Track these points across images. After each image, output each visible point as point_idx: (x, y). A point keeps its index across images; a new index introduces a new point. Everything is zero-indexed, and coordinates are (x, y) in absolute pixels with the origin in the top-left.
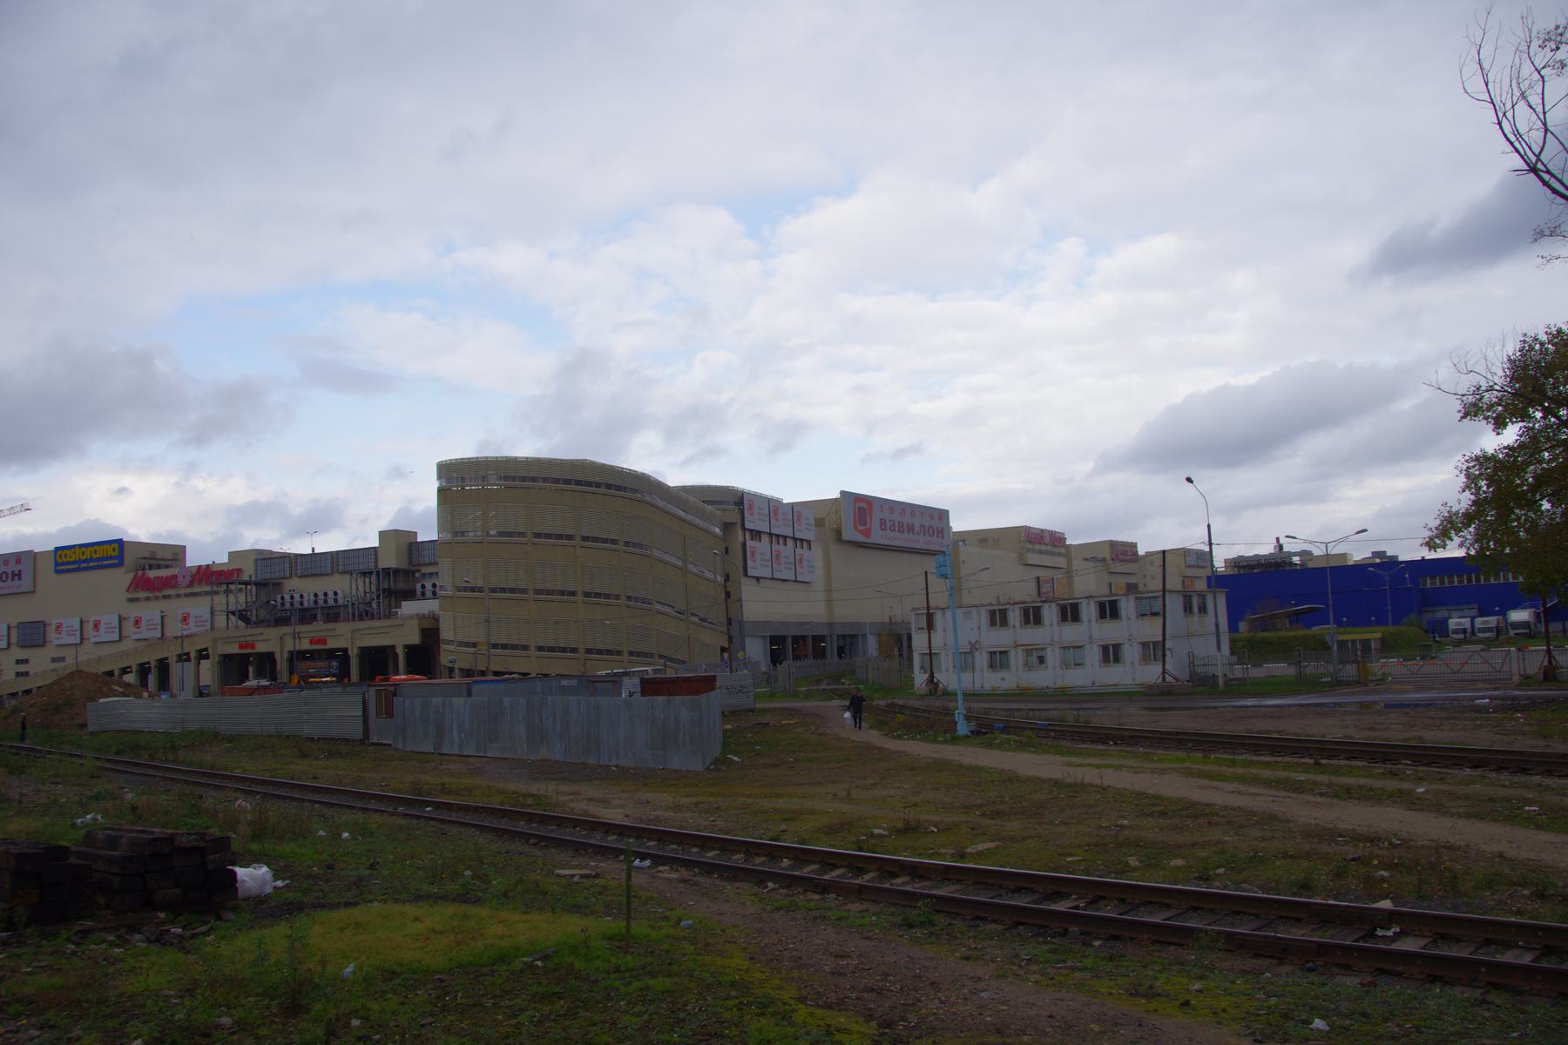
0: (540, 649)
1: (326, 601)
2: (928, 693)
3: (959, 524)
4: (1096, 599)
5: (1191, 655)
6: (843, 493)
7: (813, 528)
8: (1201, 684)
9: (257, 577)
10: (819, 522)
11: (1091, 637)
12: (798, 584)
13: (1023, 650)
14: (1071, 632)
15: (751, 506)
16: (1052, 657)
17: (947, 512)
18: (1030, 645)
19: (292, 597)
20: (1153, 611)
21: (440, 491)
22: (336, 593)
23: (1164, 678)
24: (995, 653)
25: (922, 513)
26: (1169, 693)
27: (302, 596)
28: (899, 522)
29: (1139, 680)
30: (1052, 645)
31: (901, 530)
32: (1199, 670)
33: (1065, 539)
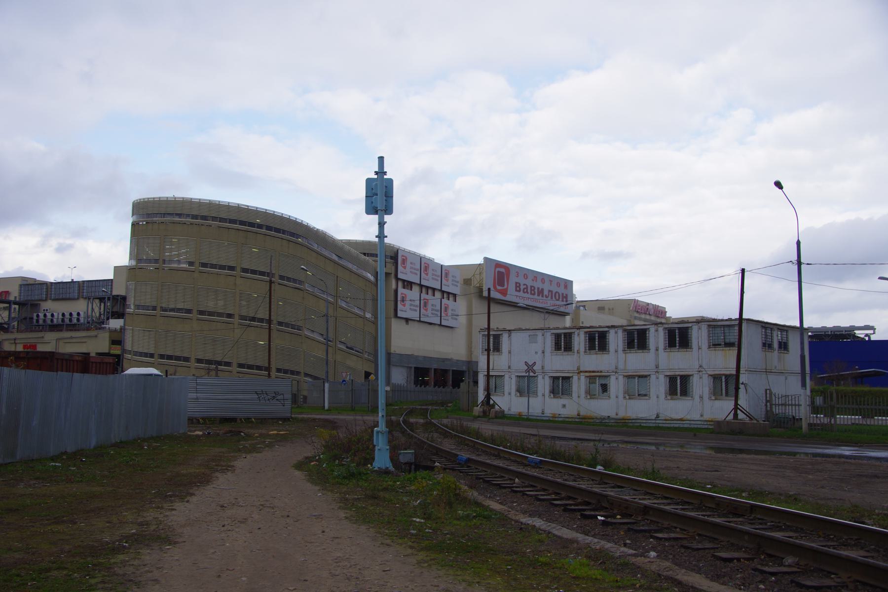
0: (241, 366)
1: (70, 320)
2: (481, 414)
3: (581, 292)
4: (666, 326)
5: (768, 392)
6: (486, 259)
7: (459, 285)
8: (190, 489)
9: (20, 299)
10: (467, 282)
11: (657, 367)
12: (442, 328)
13: (586, 377)
14: (637, 361)
15: (404, 261)
16: (616, 385)
17: (571, 282)
18: (593, 372)
19: (45, 316)
20: (727, 341)
21: (134, 225)
22: (78, 314)
23: (736, 415)
24: (557, 378)
25: (551, 281)
26: (741, 433)
27: (52, 315)
28: (531, 287)
29: (707, 417)
30: (616, 372)
31: (533, 288)
32: (777, 410)
33: (666, 312)
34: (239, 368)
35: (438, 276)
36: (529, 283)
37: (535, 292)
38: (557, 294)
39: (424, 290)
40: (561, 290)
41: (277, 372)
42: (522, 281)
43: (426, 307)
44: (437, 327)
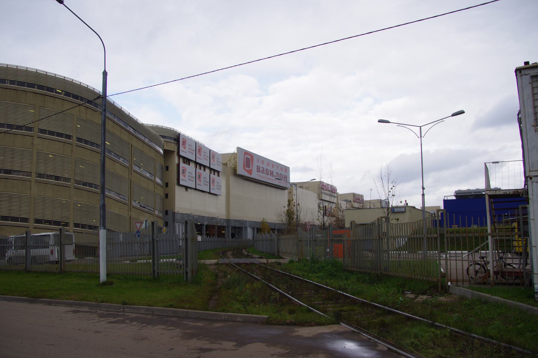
6: (239, 149)
10: (225, 164)
15: (184, 143)
25: (278, 167)
28: (266, 169)
34: (36, 223)
35: (193, 178)
36: (265, 167)
37: (268, 173)
38: (281, 175)
39: (198, 166)
40: (283, 173)
41: (75, 227)
42: (260, 164)
43: (200, 179)
44: (207, 195)
